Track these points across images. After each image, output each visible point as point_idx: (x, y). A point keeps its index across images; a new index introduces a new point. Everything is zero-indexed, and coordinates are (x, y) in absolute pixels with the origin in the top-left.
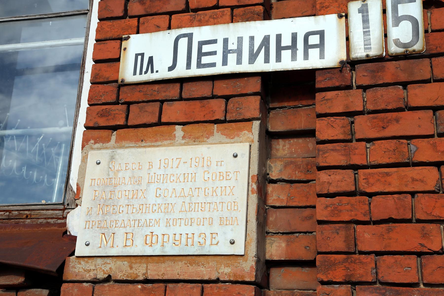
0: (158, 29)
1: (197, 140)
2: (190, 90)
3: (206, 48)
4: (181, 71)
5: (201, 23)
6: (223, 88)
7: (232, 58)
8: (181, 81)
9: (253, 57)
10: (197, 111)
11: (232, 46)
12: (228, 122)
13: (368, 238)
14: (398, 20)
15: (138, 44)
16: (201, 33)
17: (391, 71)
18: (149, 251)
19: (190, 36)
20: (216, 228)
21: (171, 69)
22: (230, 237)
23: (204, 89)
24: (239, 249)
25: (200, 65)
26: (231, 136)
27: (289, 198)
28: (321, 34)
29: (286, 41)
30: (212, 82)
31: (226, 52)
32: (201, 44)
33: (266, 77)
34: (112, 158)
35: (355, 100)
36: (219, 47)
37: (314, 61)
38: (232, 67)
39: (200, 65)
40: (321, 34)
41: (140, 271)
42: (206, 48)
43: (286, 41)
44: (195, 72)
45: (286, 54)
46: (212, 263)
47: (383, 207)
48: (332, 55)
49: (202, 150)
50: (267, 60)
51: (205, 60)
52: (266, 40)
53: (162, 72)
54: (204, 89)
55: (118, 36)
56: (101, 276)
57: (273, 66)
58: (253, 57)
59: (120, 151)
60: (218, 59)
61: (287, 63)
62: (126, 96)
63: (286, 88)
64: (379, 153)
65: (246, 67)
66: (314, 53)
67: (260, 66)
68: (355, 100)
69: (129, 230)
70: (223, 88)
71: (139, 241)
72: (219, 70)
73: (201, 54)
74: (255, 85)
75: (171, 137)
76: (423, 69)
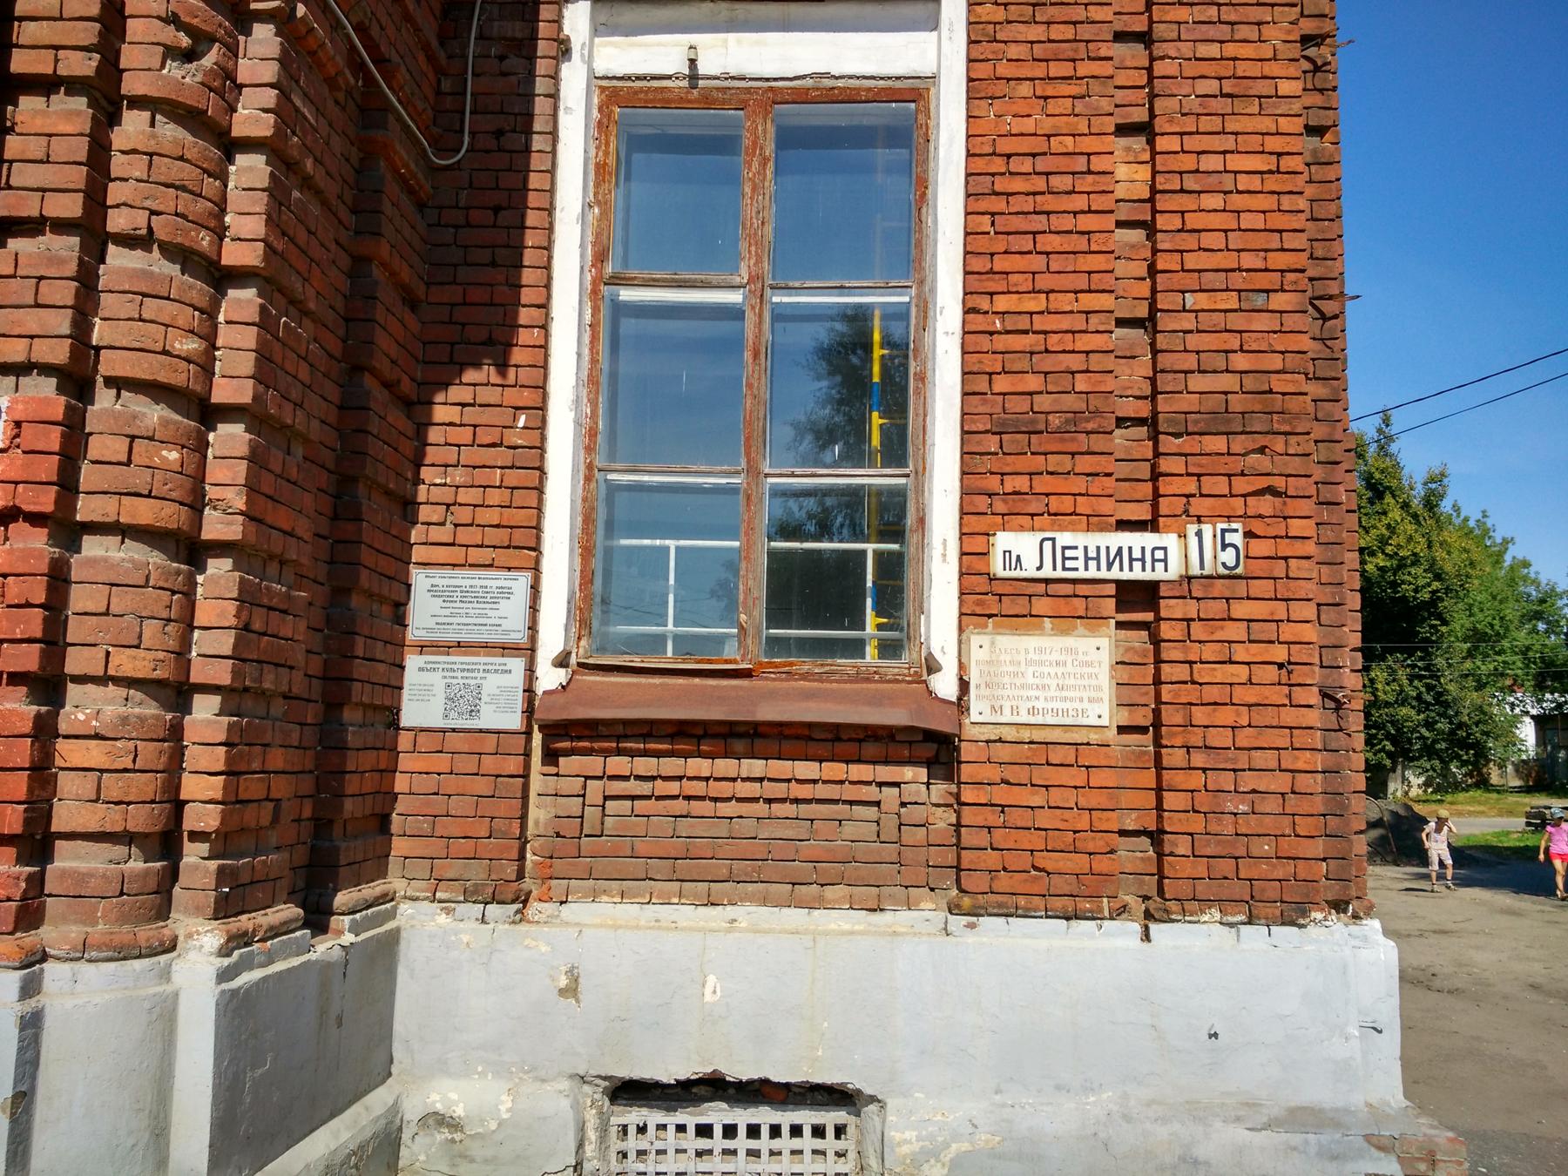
0: (1022, 528)
1: (1065, 632)
2: (1052, 588)
3: (1068, 553)
4: (1047, 572)
5: (1062, 529)
6: (1083, 589)
7: (1093, 564)
8: (1047, 581)
9: (1110, 566)
10: (1063, 607)
11: (1092, 554)
12: (1091, 618)
13: (1200, 715)
14: (1224, 546)
15: (1004, 541)
16: (1064, 538)
17: (1220, 587)
18: (1032, 720)
19: (1053, 540)
20: (1086, 705)
21: (1039, 568)
22: (1099, 712)
23: (1067, 589)
24: (1105, 722)
25: (1064, 569)
26: (1093, 632)
27: (1131, 677)
28: (1165, 549)
29: (1137, 554)
30: (125, 74)
31: (1087, 559)
32: (1064, 548)
33: (1120, 584)
34: (993, 643)
35: (1191, 609)
36: (1080, 553)
37: (1159, 574)
38: (1092, 573)
39: (1064, 569)
40: (1165, 549)
41: (1026, 735)
42: (1068, 553)
43: (1137, 554)
44: (1060, 574)
45: (1137, 565)
46: (1084, 730)
47: (1212, 693)
48: (1174, 570)
49: (1069, 641)
50: (1121, 569)
51: (1069, 564)
52: (1120, 550)
53: (1029, 571)
54: (1067, 589)
55: (1497, 835)
56: (993, 738)
57: (1126, 575)
58: (1110, 566)
59: (999, 638)
60: (1080, 564)
61: (1137, 574)
62: (999, 588)
63: (1138, 597)
64: (1209, 652)
65: (1104, 574)
66: (1160, 566)
67: (1115, 574)
68: (1191, 609)
69: (1014, 703)
70: (1083, 589)
71: (1023, 712)
72: (1081, 574)
73: (1064, 558)
74: (1111, 589)
75: (1041, 628)
76: (1241, 588)
